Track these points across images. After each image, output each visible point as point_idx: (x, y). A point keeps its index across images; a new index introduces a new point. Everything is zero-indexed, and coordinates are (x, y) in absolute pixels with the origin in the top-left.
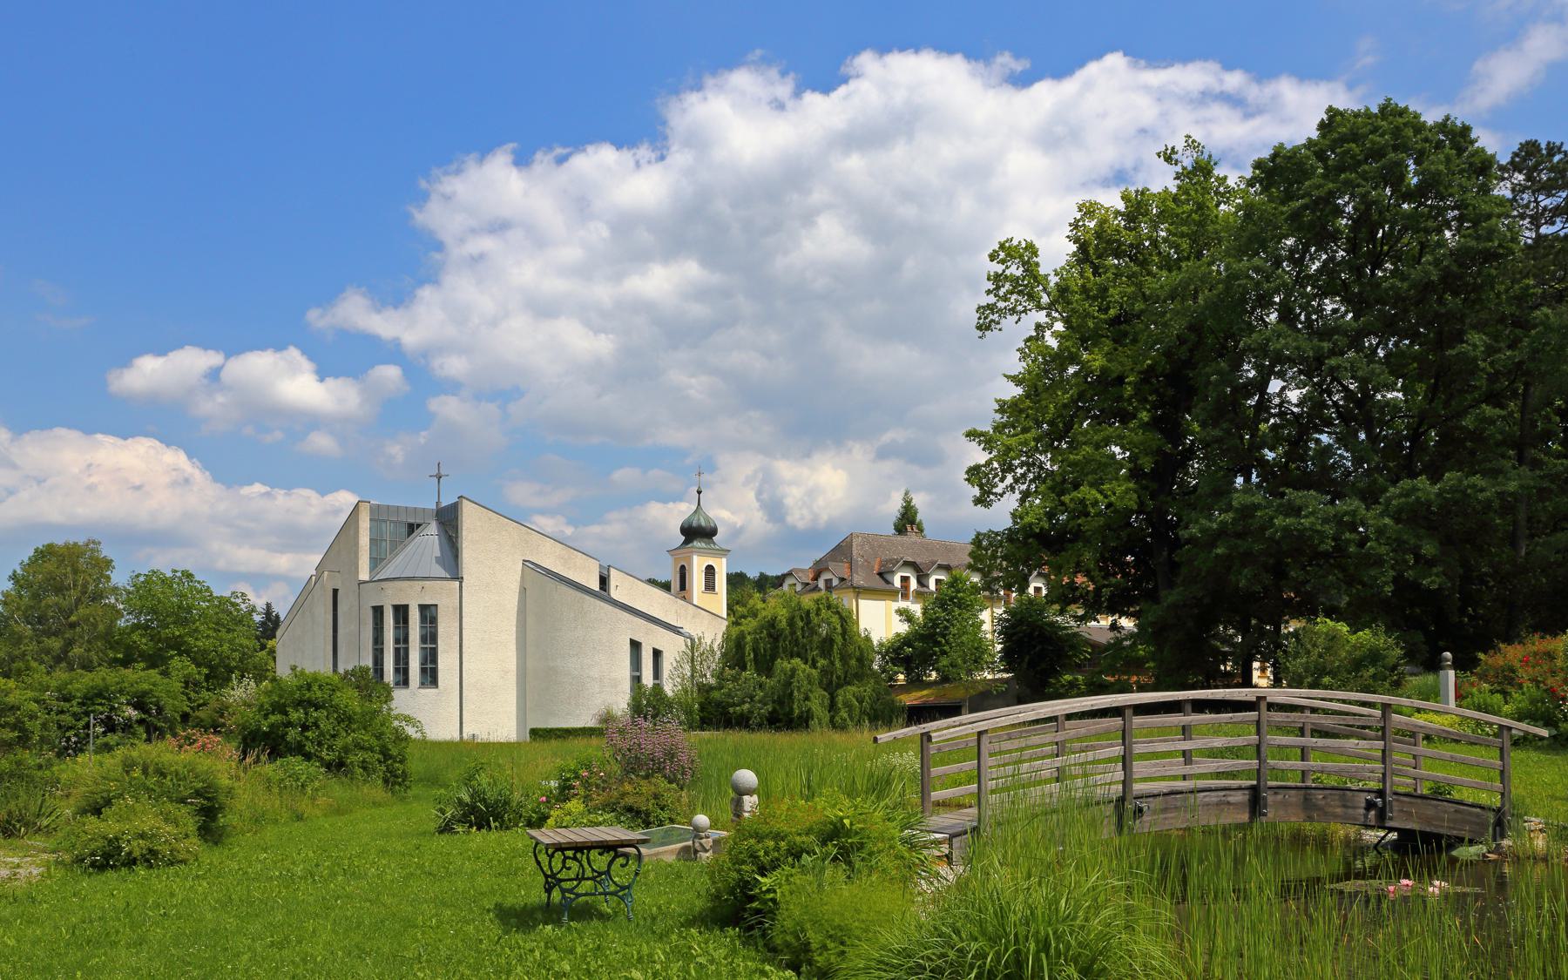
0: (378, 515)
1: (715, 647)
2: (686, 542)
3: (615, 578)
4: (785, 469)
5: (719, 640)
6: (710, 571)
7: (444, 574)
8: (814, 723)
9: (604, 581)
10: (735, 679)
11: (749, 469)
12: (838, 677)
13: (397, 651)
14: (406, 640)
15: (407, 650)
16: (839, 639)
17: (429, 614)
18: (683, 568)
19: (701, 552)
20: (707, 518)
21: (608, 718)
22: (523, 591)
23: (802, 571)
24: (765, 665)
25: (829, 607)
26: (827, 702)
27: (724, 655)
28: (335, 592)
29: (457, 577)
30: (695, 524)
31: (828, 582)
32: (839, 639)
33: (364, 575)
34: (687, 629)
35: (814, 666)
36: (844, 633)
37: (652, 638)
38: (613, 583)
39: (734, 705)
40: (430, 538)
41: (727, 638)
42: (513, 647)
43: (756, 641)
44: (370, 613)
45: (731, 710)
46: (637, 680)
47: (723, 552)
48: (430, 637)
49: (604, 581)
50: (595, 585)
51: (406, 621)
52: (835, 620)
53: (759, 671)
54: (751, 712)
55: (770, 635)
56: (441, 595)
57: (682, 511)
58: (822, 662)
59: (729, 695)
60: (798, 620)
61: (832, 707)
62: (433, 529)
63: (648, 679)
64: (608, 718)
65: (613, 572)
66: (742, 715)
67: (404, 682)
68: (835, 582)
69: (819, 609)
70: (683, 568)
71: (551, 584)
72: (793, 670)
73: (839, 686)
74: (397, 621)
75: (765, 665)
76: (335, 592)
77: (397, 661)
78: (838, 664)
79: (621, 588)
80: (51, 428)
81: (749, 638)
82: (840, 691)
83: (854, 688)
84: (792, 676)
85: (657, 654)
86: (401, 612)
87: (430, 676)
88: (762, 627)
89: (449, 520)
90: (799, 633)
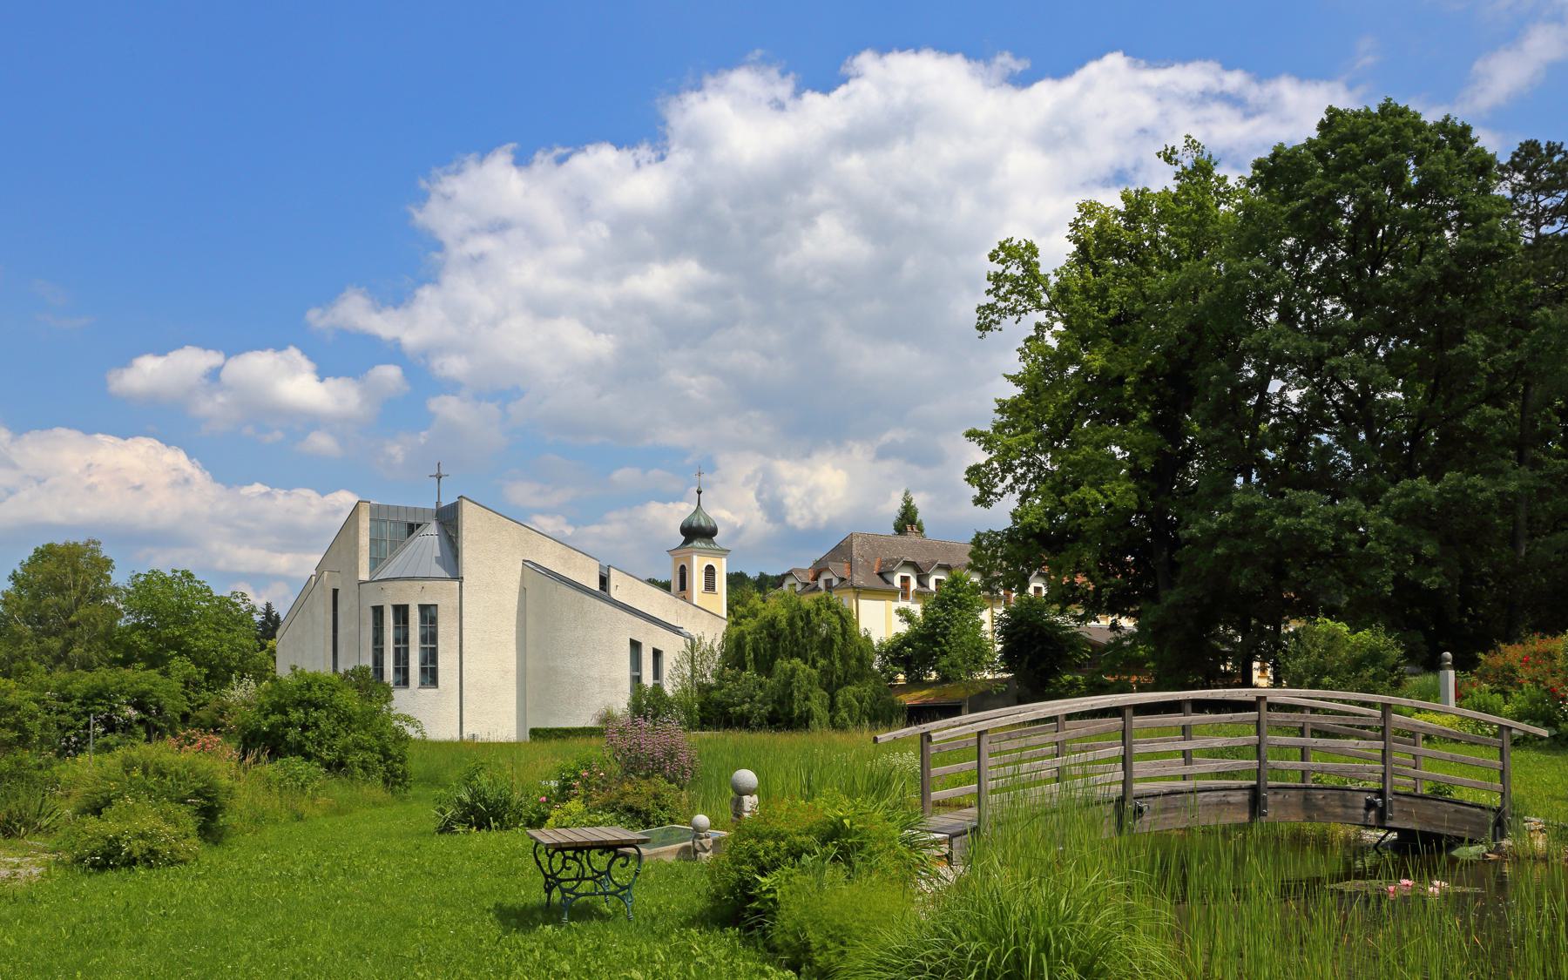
0: (378, 515)
1: (715, 647)
2: (686, 542)
3: (615, 578)
4: (785, 469)
5: (719, 640)
6: (710, 571)
7: (444, 574)
8: (814, 723)
9: (604, 581)
10: (735, 679)
11: (749, 469)
12: (838, 677)
13: (397, 651)
14: (406, 640)
15: (407, 650)
16: (839, 639)
17: (429, 614)
18: (683, 568)
19: (701, 552)
20: (707, 518)
21: (608, 718)
22: (523, 591)
23: (802, 571)
24: (765, 665)
25: (829, 607)
26: (827, 702)
27: (724, 655)
28: (335, 592)
29: (457, 577)
30: (695, 524)
31: (828, 582)
32: (839, 639)
33: (364, 575)
34: (687, 629)
35: (814, 666)
36: (844, 633)
37: (652, 638)
38: (613, 583)
39: (734, 705)
40: (430, 538)
41: (727, 638)
42: (513, 647)
43: (756, 641)
44: (370, 613)
45: (731, 710)
46: (637, 680)
47: (723, 552)
48: (430, 637)
49: (604, 581)
50: (595, 585)
51: (406, 621)
52: (835, 620)
53: (759, 671)
54: (751, 712)
55: (770, 635)
56: (441, 595)
58: (822, 662)
59: (729, 695)
60: (798, 620)
61: (832, 707)
62: (433, 529)
63: (648, 679)
64: (608, 718)
65: (613, 572)
66: (742, 715)
67: (404, 682)
68: (835, 582)
69: (819, 609)
70: (683, 568)
71: (551, 584)
72: (793, 670)
73: (839, 686)
74: (397, 621)
75: (765, 665)
76: (335, 592)
77: (397, 661)
78: (838, 664)
79: (621, 588)
81: (749, 638)
82: (840, 691)
83: (854, 688)
84: (792, 676)
85: (657, 654)
86: (401, 612)
87: (430, 676)
88: (762, 627)
89: (449, 520)
90: (799, 633)
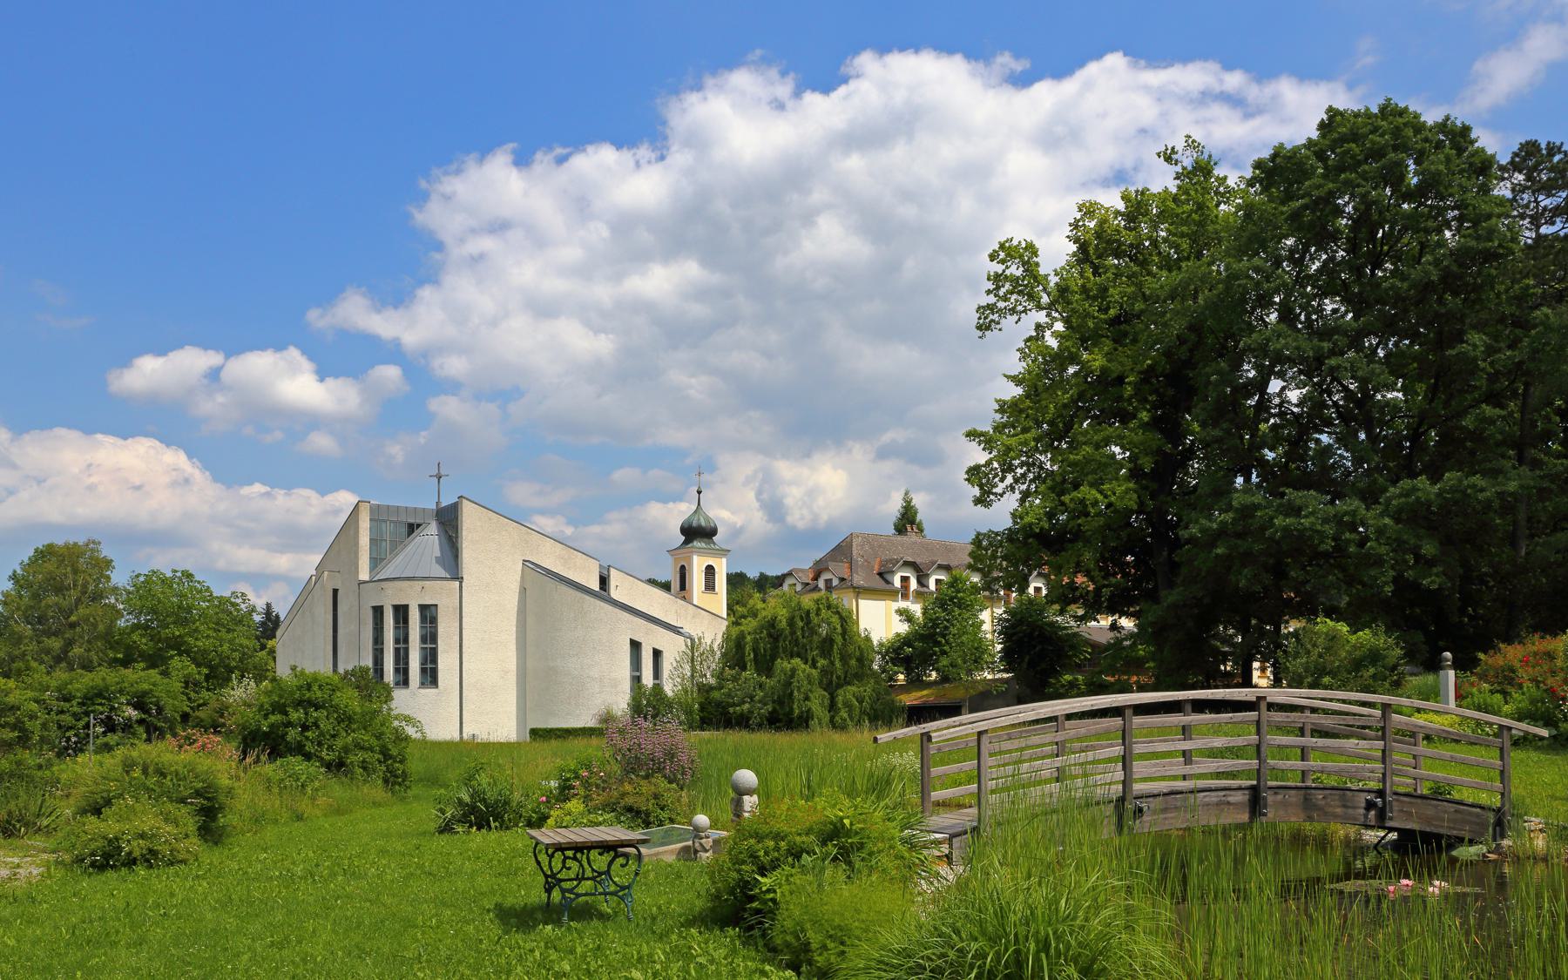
0: (378, 515)
1: (715, 647)
2: (686, 542)
3: (615, 578)
4: (785, 469)
5: (719, 640)
6: (710, 571)
7: (444, 574)
8: (814, 723)
9: (604, 581)
10: (735, 679)
11: (749, 469)
12: (838, 677)
13: (397, 651)
14: (406, 640)
15: (407, 650)
16: (839, 639)
17: (429, 614)
18: (683, 568)
19: (701, 552)
20: (707, 518)
21: (608, 718)
22: (523, 591)
23: (802, 571)
24: (765, 665)
25: (829, 607)
26: (827, 702)
27: (724, 655)
28: (335, 592)
29: (457, 577)
30: (695, 524)
31: (828, 582)
32: (839, 639)
33: (364, 575)
34: (687, 629)
35: (814, 666)
36: (844, 633)
37: (652, 638)
38: (613, 583)
39: (734, 705)
40: (430, 538)
41: (727, 638)
42: (513, 647)
43: (756, 641)
44: (370, 613)
45: (731, 710)
46: (637, 680)
47: (723, 552)
48: (430, 637)
49: (604, 581)
50: (595, 585)
51: (406, 621)
52: (835, 620)
53: (759, 671)
54: (751, 712)
55: (770, 635)
56: (441, 595)
57: (682, 511)
58: (822, 662)
59: (729, 695)
60: (798, 620)
61: (832, 707)
62: (433, 529)
63: (648, 679)
64: (608, 718)
65: (613, 572)
66: (742, 715)
67: (404, 682)
68: (835, 582)
69: (819, 609)
70: (683, 568)
71: (551, 584)
72: (793, 670)
73: (839, 686)
74: (397, 621)
75: (765, 665)
76: (335, 592)
77: (397, 661)
78: (838, 664)
79: (621, 588)
80: (51, 428)
81: (749, 638)
82: (840, 691)
83: (854, 688)
84: (792, 676)
85: (657, 654)
86: (401, 612)
87: (430, 676)
88: (762, 627)
89: (449, 520)
90: (799, 633)
